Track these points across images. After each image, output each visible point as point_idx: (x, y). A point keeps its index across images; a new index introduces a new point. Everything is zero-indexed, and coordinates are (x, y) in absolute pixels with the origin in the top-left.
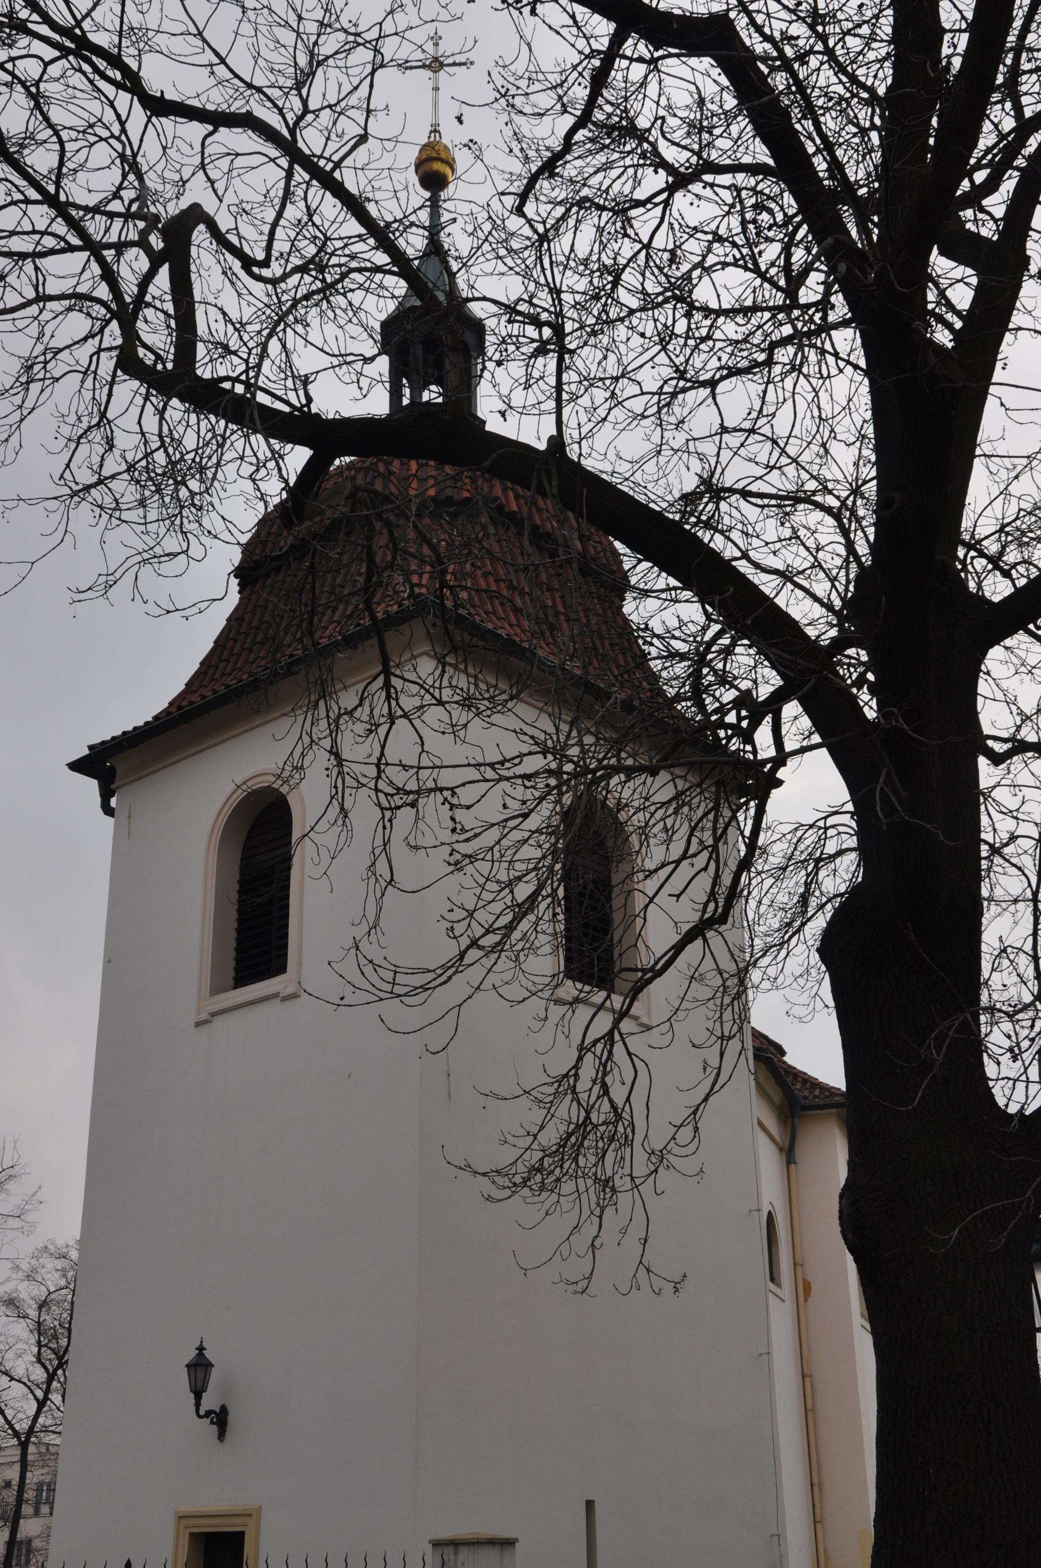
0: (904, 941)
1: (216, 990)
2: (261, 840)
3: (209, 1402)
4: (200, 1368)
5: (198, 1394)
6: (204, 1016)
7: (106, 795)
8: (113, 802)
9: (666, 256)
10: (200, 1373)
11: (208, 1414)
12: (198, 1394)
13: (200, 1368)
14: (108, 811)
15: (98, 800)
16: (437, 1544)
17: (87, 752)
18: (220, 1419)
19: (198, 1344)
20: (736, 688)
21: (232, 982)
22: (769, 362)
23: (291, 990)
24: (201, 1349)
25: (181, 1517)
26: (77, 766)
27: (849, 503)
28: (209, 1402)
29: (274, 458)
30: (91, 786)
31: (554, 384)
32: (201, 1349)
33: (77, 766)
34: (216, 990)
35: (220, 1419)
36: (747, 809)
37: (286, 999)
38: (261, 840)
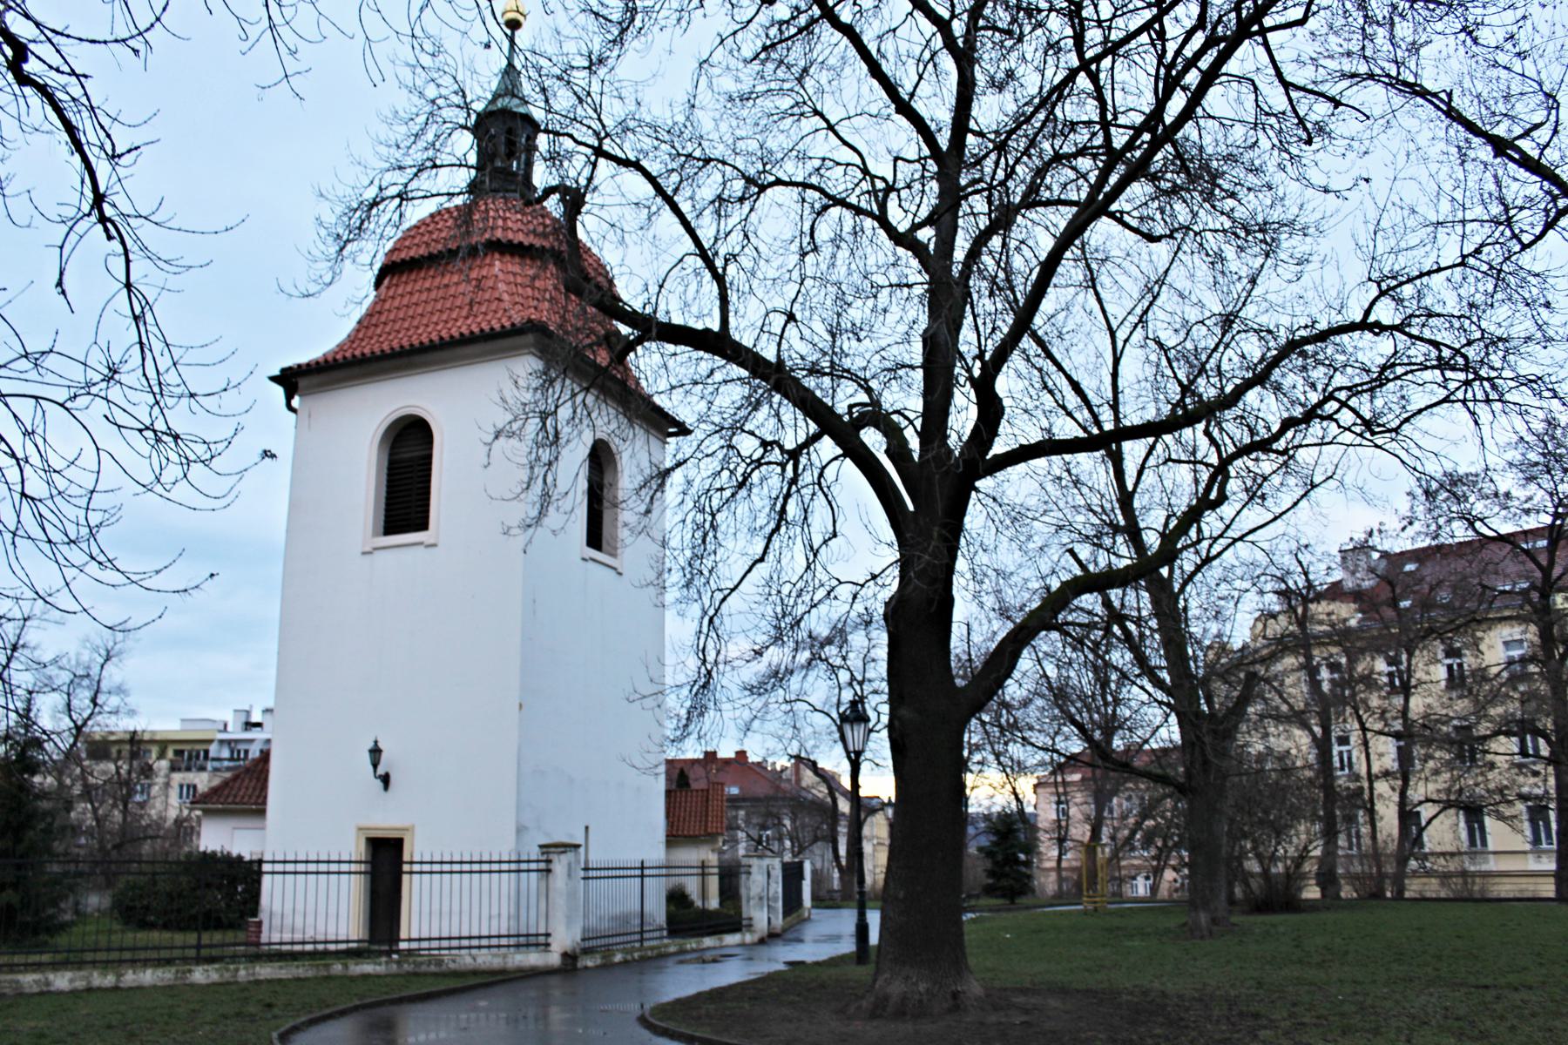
1: (375, 534)
2: (409, 445)
4: (376, 752)
5: (375, 766)
6: (368, 549)
7: (289, 398)
8: (295, 402)
13: (376, 752)
15: (283, 401)
16: (541, 846)
17: (733, 755)
18: (386, 780)
19: (371, 745)
20: (1107, 603)
22: (1489, 379)
23: (432, 541)
25: (360, 829)
26: (273, 379)
28: (381, 771)
29: (1396, 78)
30: (279, 391)
31: (1043, 256)
34: (375, 534)
35: (386, 780)
38: (409, 445)
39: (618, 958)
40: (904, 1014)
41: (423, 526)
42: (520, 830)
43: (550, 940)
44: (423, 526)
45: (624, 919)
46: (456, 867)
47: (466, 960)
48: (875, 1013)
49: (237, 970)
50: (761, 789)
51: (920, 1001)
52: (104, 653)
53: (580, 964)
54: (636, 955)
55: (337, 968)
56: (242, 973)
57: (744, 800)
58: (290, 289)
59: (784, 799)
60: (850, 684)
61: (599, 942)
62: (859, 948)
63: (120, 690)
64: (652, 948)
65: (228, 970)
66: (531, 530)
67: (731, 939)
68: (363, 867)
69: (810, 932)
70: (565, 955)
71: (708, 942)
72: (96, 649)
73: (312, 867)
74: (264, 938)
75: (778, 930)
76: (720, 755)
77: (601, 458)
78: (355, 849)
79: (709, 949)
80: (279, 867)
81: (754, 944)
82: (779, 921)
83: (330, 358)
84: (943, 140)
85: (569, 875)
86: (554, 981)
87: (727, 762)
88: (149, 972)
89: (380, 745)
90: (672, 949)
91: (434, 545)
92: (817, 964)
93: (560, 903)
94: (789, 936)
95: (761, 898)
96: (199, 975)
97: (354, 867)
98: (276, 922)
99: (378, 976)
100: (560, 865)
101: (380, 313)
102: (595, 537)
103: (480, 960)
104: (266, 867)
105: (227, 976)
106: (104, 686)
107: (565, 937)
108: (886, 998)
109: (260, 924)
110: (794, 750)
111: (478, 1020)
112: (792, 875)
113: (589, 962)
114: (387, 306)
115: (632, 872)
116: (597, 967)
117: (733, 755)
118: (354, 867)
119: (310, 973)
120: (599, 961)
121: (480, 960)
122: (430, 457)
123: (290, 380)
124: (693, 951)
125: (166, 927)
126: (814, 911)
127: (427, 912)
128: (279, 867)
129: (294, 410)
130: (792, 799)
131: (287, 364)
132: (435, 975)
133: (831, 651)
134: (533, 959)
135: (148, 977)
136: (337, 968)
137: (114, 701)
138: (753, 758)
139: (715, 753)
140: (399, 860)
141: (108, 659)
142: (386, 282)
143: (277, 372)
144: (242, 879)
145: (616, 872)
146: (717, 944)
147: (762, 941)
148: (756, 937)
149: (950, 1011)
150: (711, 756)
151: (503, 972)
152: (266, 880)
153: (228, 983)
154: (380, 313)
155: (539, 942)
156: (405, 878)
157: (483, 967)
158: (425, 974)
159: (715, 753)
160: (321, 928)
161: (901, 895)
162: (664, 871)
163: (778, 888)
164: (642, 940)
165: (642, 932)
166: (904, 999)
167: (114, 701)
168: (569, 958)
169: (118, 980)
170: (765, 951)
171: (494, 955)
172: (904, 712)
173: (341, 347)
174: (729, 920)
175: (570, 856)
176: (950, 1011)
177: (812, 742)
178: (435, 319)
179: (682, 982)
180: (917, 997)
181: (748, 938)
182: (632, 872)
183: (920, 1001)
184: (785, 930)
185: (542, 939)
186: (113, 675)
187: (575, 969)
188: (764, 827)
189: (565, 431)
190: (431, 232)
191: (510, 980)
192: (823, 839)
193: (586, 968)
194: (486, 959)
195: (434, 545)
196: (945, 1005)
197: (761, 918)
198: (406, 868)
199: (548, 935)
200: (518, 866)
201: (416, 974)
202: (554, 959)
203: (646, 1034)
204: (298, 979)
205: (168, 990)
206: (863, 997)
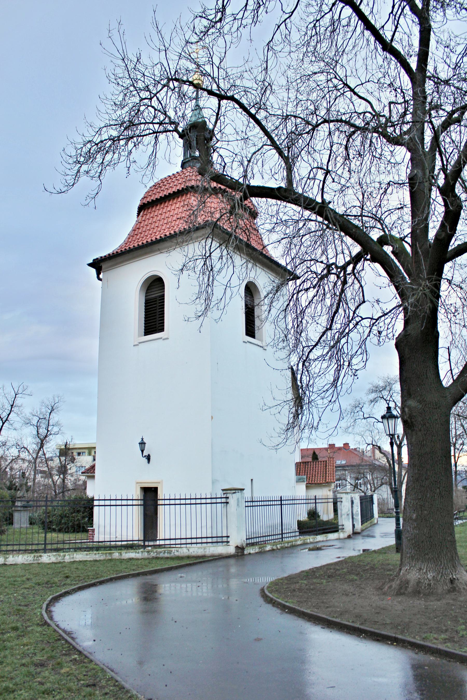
0: (418, 346)
1: (139, 336)
3: (145, 453)
4: (142, 444)
5: (142, 451)
6: (136, 343)
7: (98, 274)
8: (101, 276)
9: (446, 49)
10: (143, 445)
11: (145, 456)
12: (142, 451)
13: (142, 444)
14: (99, 279)
16: (223, 490)
17: (342, 446)
19: (140, 440)
21: (143, 334)
24: (142, 439)
26: (90, 265)
27: (196, 213)
28: (145, 453)
30: (93, 271)
32: (142, 439)
33: (90, 265)
34: (139, 336)
36: (444, 169)
37: (164, 339)
39: (268, 548)
40: (419, 592)
41: (162, 330)
42: (214, 482)
43: (229, 539)
44: (162, 330)
45: (273, 527)
46: (124, 503)
47: (184, 551)
48: (401, 591)
49: (65, 556)
50: (355, 461)
51: (429, 585)
52: (50, 408)
53: (246, 552)
54: (279, 546)
55: (116, 555)
56: (67, 557)
57: (348, 466)
58: (50, 189)
59: (366, 465)
60: (395, 408)
61: (260, 539)
62: (397, 543)
63: (57, 424)
64: (288, 542)
65: (60, 556)
66: (201, 318)
67: (332, 536)
68: (139, 502)
69: (378, 531)
70: (237, 547)
71: (320, 538)
72: (47, 407)
73: (198, 501)
74: (96, 539)
75: (359, 530)
76: (336, 446)
77: (250, 290)
78: (137, 494)
79: (319, 542)
80: (102, 503)
81: (345, 539)
82: (359, 526)
83: (115, 252)
84: (413, 63)
85: (238, 505)
86: (232, 561)
87: (339, 449)
88: (21, 556)
89: (145, 440)
90: (299, 543)
91: (167, 339)
92: (375, 551)
93: (233, 519)
94: (365, 533)
95: (348, 515)
96: (46, 558)
97: (135, 502)
98: (102, 529)
99: (138, 559)
100: (233, 499)
101: (139, 228)
102: (250, 331)
103: (191, 550)
104: (96, 503)
105: (60, 559)
106: (51, 423)
107: (238, 538)
108: (407, 582)
109: (93, 531)
110: (369, 440)
111: (170, 587)
112: (366, 502)
113: (252, 550)
114: (142, 225)
115: (321, 501)
116: (256, 553)
117: (342, 446)
118: (135, 502)
119: (102, 558)
120: (257, 550)
121: (191, 550)
122: (163, 295)
123: (98, 265)
124: (311, 543)
125: (60, 531)
126: (380, 519)
127: (170, 524)
128: (102, 503)
129: (100, 279)
130: (370, 465)
131: (95, 258)
132: (167, 558)
133: (385, 393)
134: (220, 550)
135: (20, 559)
136: (116, 555)
137: (56, 429)
138: (352, 446)
139: (334, 445)
140: (156, 499)
141: (52, 410)
142: (141, 214)
143: (91, 261)
144: (87, 507)
145: (266, 503)
146: (325, 539)
147: (349, 537)
148: (346, 535)
149: (449, 591)
150: (332, 446)
151: (203, 557)
152: (96, 509)
153: (60, 563)
154: (139, 228)
155: (224, 540)
156: (160, 509)
157: (194, 554)
158: (162, 558)
159: (334, 445)
160: (124, 533)
161: (414, 516)
162: (304, 501)
163: (357, 508)
164: (282, 538)
165: (282, 534)
166: (419, 583)
167: (56, 429)
168: (240, 549)
169: (5, 561)
170: (351, 543)
171: (199, 548)
172: (412, 403)
173: (121, 247)
174: (332, 527)
175: (238, 495)
176: (449, 591)
177: (378, 437)
178: (164, 228)
179: (306, 561)
180: (427, 582)
181: (342, 535)
182: (321, 501)
183: (429, 585)
184: (362, 531)
185: (225, 539)
186: (55, 418)
187: (243, 555)
188: (357, 479)
189: (217, 267)
190: (161, 187)
191: (216, 559)
192: (386, 483)
193: (250, 554)
194: (196, 550)
195: (167, 339)
196: (446, 587)
197: (347, 524)
198: (160, 502)
199: (228, 537)
200: (212, 500)
201: (157, 558)
202: (231, 550)
203: (261, 600)
204: (96, 561)
205: (25, 566)
206: (393, 580)
